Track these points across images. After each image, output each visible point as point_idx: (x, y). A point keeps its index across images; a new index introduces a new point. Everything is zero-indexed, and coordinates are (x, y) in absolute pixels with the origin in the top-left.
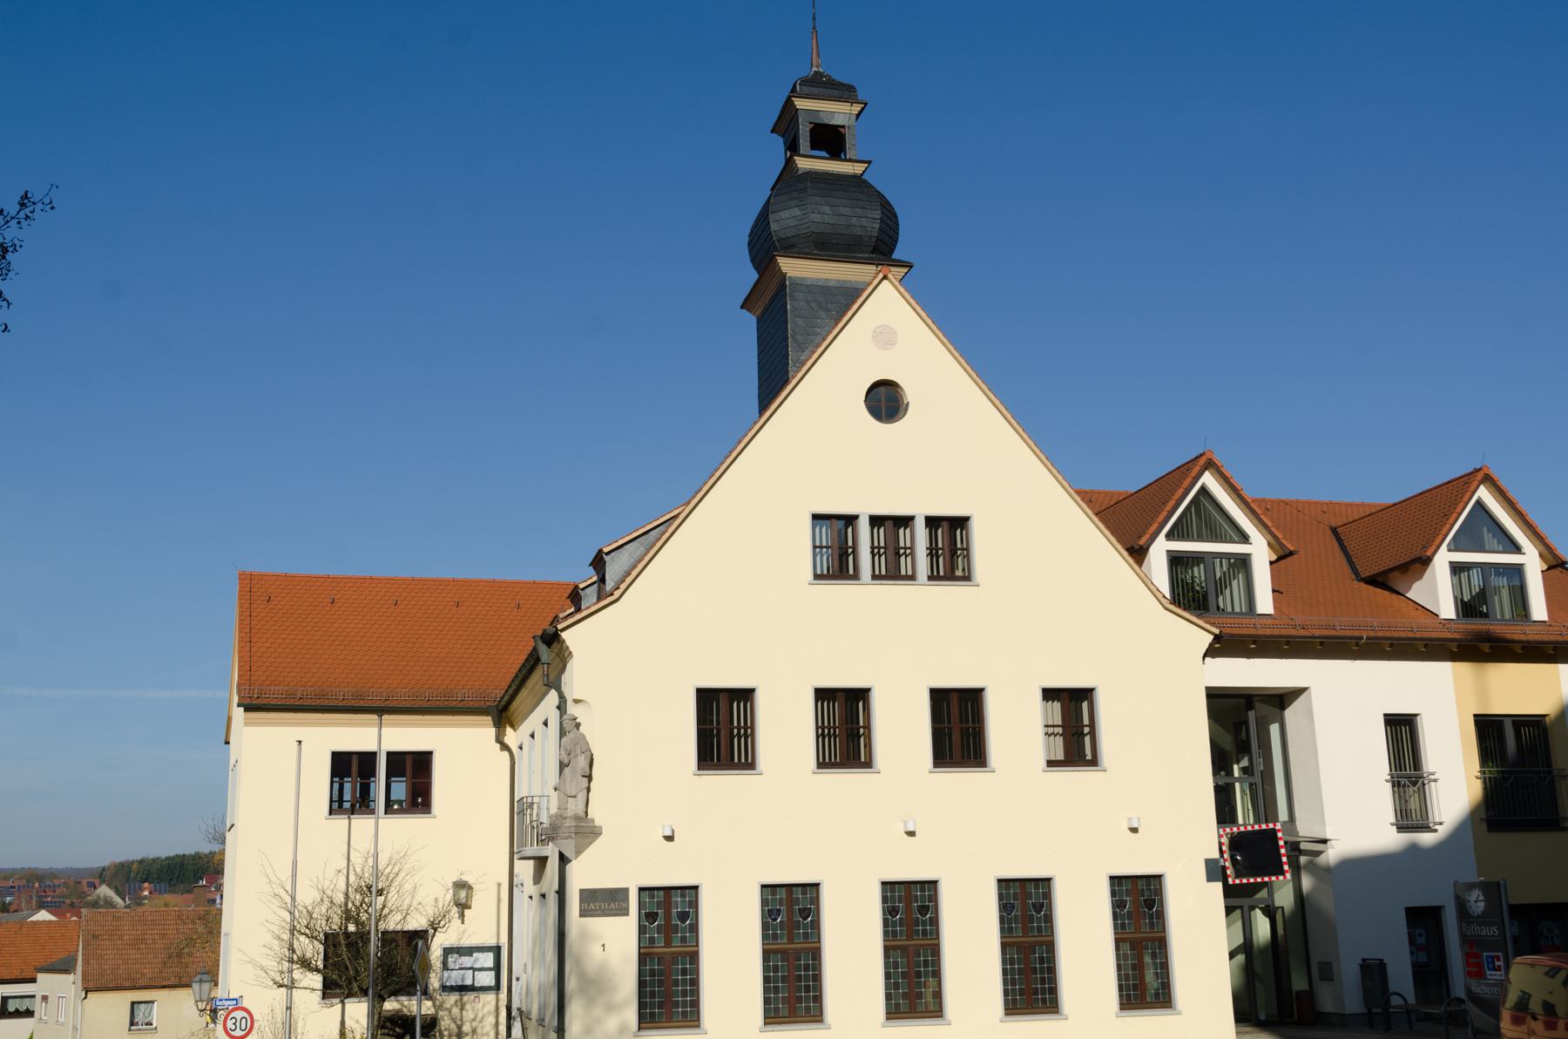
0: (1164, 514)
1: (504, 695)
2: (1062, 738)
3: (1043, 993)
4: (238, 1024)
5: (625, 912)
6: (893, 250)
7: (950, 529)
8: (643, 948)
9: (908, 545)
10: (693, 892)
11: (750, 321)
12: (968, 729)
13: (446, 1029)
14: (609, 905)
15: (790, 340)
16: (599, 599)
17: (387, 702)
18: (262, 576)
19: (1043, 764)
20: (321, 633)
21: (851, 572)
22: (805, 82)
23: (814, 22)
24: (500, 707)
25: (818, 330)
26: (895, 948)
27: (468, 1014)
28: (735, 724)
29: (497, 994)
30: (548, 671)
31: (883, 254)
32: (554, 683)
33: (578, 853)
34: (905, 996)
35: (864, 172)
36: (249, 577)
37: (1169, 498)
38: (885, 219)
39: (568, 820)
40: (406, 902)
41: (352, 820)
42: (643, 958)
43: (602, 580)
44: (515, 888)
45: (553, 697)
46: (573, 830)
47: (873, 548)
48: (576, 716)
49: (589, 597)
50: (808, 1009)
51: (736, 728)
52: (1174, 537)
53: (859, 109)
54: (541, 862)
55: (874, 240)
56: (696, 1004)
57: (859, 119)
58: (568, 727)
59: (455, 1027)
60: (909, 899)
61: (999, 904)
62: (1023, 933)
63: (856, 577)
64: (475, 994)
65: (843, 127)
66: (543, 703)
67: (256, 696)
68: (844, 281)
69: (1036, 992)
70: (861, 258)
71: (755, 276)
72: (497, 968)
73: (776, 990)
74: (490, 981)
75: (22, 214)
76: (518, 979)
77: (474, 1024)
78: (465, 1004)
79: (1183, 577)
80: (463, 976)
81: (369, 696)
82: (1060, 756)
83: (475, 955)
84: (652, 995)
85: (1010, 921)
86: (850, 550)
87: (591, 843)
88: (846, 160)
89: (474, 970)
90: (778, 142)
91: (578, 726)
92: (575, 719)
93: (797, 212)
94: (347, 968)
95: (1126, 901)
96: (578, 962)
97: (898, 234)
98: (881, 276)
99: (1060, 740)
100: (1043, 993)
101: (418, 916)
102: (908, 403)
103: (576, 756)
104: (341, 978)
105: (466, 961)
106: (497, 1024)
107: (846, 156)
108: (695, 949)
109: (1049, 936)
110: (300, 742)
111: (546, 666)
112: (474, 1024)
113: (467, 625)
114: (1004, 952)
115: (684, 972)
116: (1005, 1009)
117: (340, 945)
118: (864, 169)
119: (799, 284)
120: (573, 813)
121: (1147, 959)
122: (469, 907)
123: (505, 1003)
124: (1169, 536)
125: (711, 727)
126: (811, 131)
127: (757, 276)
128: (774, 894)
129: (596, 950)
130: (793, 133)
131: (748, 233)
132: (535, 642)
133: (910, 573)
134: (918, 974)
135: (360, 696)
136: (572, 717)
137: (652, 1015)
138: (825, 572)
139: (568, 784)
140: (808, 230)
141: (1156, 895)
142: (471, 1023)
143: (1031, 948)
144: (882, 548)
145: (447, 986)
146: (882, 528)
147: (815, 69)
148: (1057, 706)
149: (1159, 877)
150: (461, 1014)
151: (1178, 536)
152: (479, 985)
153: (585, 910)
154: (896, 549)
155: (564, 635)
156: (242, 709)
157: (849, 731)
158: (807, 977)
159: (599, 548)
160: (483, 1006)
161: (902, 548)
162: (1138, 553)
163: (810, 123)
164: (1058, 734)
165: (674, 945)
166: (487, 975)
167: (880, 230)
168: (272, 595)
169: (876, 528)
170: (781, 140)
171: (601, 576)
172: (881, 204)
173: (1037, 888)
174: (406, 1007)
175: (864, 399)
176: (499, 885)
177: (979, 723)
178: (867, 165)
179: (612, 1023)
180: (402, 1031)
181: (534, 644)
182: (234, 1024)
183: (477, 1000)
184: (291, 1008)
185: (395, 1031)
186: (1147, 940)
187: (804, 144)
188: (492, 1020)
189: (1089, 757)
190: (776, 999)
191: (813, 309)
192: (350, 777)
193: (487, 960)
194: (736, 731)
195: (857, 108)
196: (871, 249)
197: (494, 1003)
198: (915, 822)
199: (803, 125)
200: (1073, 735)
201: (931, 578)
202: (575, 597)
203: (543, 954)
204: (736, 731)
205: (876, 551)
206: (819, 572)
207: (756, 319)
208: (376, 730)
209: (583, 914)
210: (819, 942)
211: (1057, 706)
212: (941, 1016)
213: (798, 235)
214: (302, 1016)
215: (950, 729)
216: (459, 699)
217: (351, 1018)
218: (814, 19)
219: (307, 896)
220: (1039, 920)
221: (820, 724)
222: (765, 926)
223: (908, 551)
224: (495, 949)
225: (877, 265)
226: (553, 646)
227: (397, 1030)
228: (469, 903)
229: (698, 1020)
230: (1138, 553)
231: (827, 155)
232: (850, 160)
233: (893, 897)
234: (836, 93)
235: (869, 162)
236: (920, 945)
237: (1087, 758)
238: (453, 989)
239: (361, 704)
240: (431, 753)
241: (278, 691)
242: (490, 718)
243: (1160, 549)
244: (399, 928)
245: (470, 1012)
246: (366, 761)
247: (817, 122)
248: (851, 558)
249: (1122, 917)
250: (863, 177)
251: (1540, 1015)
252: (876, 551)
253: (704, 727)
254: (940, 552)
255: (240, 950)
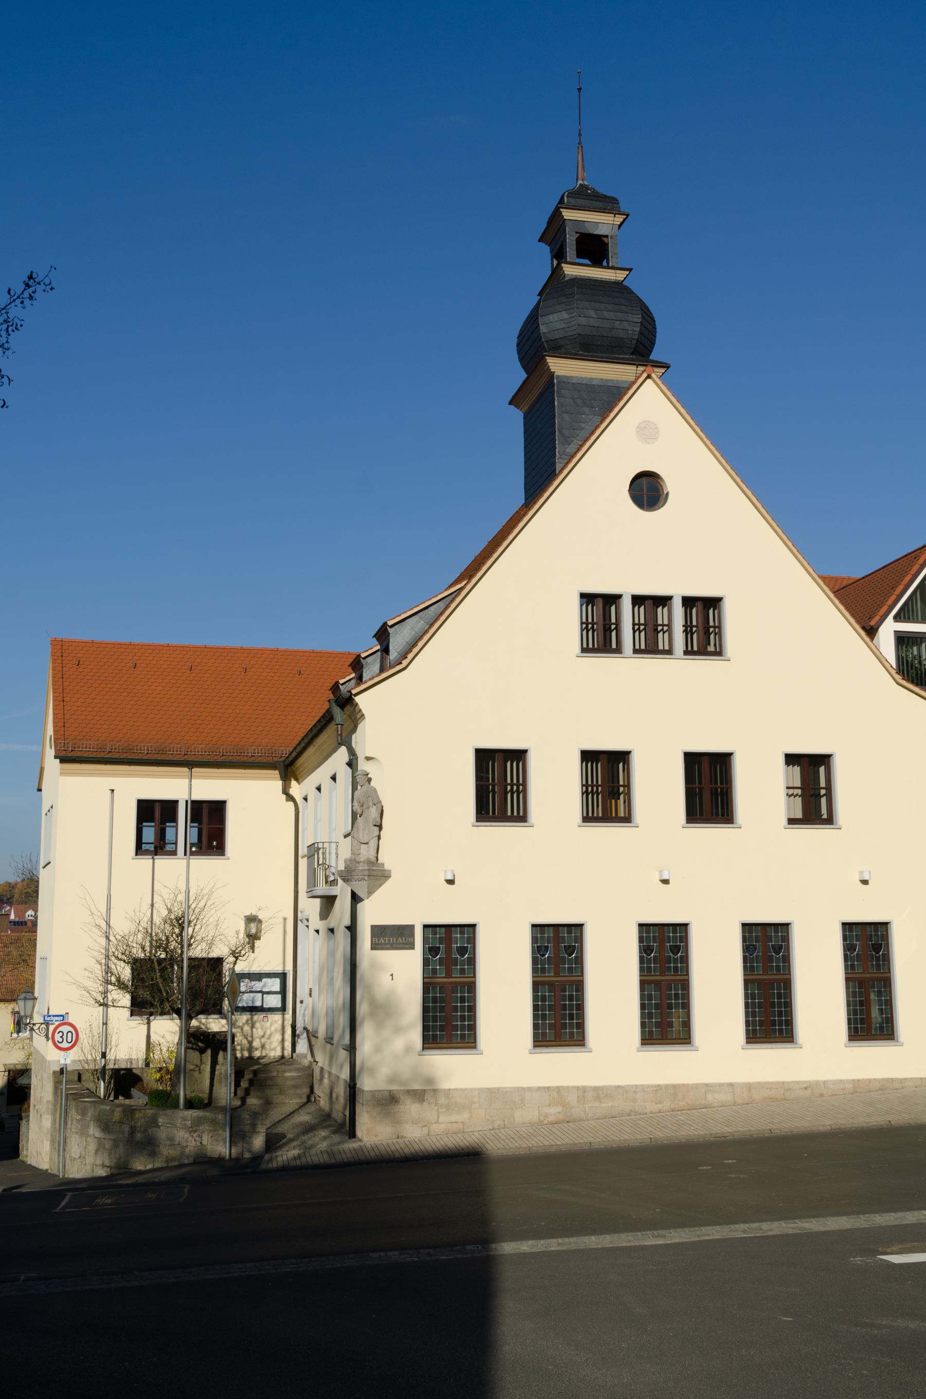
0: (893, 598)
1: (292, 752)
2: (801, 798)
3: (780, 1024)
4: (65, 1037)
5: (411, 946)
6: (651, 352)
7: (704, 609)
8: (426, 978)
9: (666, 622)
10: (471, 929)
11: (517, 417)
12: (716, 789)
13: (238, 1044)
14: (397, 940)
15: (557, 433)
16: (382, 670)
17: (186, 757)
18: (71, 643)
19: (784, 821)
20: (125, 694)
21: (614, 646)
22: (572, 194)
23: (580, 139)
24: (287, 762)
25: (583, 425)
26: (649, 982)
27: (258, 1032)
28: (509, 781)
29: (283, 1014)
30: (341, 731)
31: (642, 356)
32: (345, 741)
33: (370, 893)
34: (658, 1025)
35: (625, 279)
36: (60, 643)
37: (898, 583)
38: (645, 323)
39: (361, 864)
40: (211, 934)
41: (156, 860)
42: (427, 987)
43: (386, 650)
44: (299, 922)
45: (342, 754)
46: (366, 873)
47: (634, 624)
48: (368, 771)
49: (371, 668)
50: (572, 1034)
51: (509, 784)
52: (900, 618)
53: (622, 220)
54: (329, 902)
55: (634, 342)
56: (473, 1028)
57: (620, 229)
58: (359, 780)
59: (246, 1042)
60: (662, 940)
61: (743, 945)
62: (763, 972)
63: (618, 650)
64: (264, 1014)
65: (607, 236)
66: (330, 759)
67: (70, 749)
68: (607, 380)
69: (773, 1023)
70: (622, 359)
71: (525, 376)
72: (283, 992)
73: (544, 1017)
74: (278, 1002)
75: (26, 294)
76: (302, 1002)
77: (263, 1040)
78: (255, 1022)
79: (904, 655)
80: (253, 998)
81: (170, 751)
82: (799, 815)
83: (264, 980)
84: (435, 1019)
85: (752, 961)
86: (613, 627)
87: (381, 885)
88: (608, 267)
89: (263, 993)
90: (545, 250)
91: (369, 780)
92: (368, 774)
93: (565, 315)
94: (160, 991)
95: (856, 945)
96: (369, 989)
97: (655, 337)
98: (645, 375)
99: (799, 800)
100: (780, 1024)
101: (221, 946)
102: (668, 494)
103: (368, 808)
104: (154, 997)
105: (257, 985)
106: (283, 1040)
107: (608, 263)
108: (472, 979)
109: (787, 974)
110: (113, 791)
111: (339, 726)
112: (263, 1040)
113: (254, 688)
114: (642, 989)
115: (463, 999)
116: (747, 1038)
117: (155, 971)
118: (625, 276)
119: (566, 382)
120: (365, 858)
121: (873, 997)
122: (259, 939)
123: (290, 1022)
124: (897, 618)
125: (487, 783)
126: (577, 240)
127: (525, 376)
128: (542, 932)
129: (385, 979)
130: (559, 244)
131: (517, 336)
132: (330, 704)
133: (667, 648)
134: (670, 1006)
135: (162, 750)
136: (366, 773)
137: (435, 1037)
138: (591, 646)
139: (361, 833)
140: (574, 332)
141: (882, 940)
142: (260, 1039)
143: (770, 985)
144: (642, 624)
145: (239, 1007)
146: (643, 607)
147: (580, 182)
148: (797, 770)
149: (885, 925)
150: (252, 1031)
151: (905, 618)
152: (267, 1007)
153: (376, 944)
154: (654, 626)
155: (357, 699)
156: (58, 760)
157: (611, 789)
158: (571, 1006)
159: (384, 621)
160: (271, 1025)
161: (660, 625)
162: (871, 632)
163: (577, 233)
164: (797, 795)
165: (453, 976)
166: (275, 998)
167: (641, 333)
168: (81, 659)
169: (637, 607)
170: (547, 248)
171: (384, 646)
172: (642, 310)
173: (776, 932)
174: (203, 1024)
175: (628, 488)
176: (285, 919)
177: (726, 784)
178: (628, 272)
179: (399, 1044)
180: (204, 1046)
181: (327, 708)
182: (62, 1037)
183: (265, 1020)
184: (106, 1024)
185: (198, 1045)
186: (873, 979)
187: (571, 251)
188: (278, 1037)
189: (825, 816)
190: (544, 1025)
191: (578, 406)
192: (153, 822)
193: (275, 984)
194: (509, 788)
195: (619, 219)
196: (632, 350)
197: (280, 1022)
198: (669, 871)
199: (569, 234)
200: (812, 796)
201: (686, 653)
202: (357, 665)
203: (331, 980)
204: (509, 788)
205: (636, 627)
206: (637, 647)
207: (523, 414)
208: (187, 781)
209: (374, 947)
210: (582, 975)
211: (797, 770)
212: (689, 1043)
213: (565, 337)
214: (116, 1031)
215: (701, 789)
216: (250, 754)
217: (156, 1033)
218: (580, 135)
219: (122, 926)
220: (778, 960)
221: (584, 783)
222: (535, 961)
223: (665, 628)
224: (282, 975)
225: (637, 366)
226: (346, 709)
227: (200, 1044)
228: (259, 934)
229: (475, 1042)
230: (871, 632)
231: (589, 263)
232: (613, 268)
233: (648, 938)
234: (600, 204)
235: (630, 270)
236: (459, 983)
237: (823, 817)
238: (244, 1009)
239: (163, 757)
240: (224, 802)
241: (90, 745)
242: (277, 772)
243: (889, 629)
244: (204, 955)
245: (260, 1030)
246: (168, 809)
247: (582, 231)
248: (614, 634)
249: (852, 959)
250: (624, 283)
251: (275, 1054)
252: (636, 627)
253: (482, 783)
254: (694, 629)
255: (66, 973)
